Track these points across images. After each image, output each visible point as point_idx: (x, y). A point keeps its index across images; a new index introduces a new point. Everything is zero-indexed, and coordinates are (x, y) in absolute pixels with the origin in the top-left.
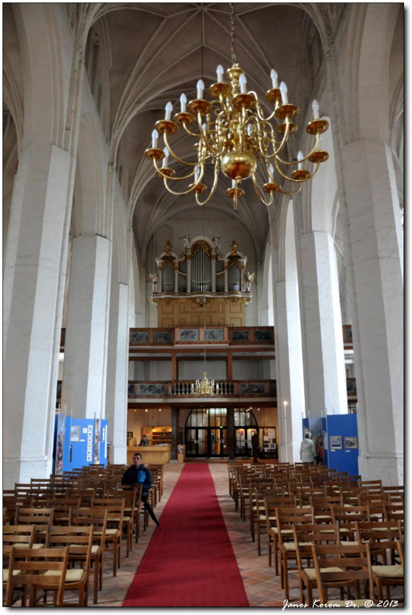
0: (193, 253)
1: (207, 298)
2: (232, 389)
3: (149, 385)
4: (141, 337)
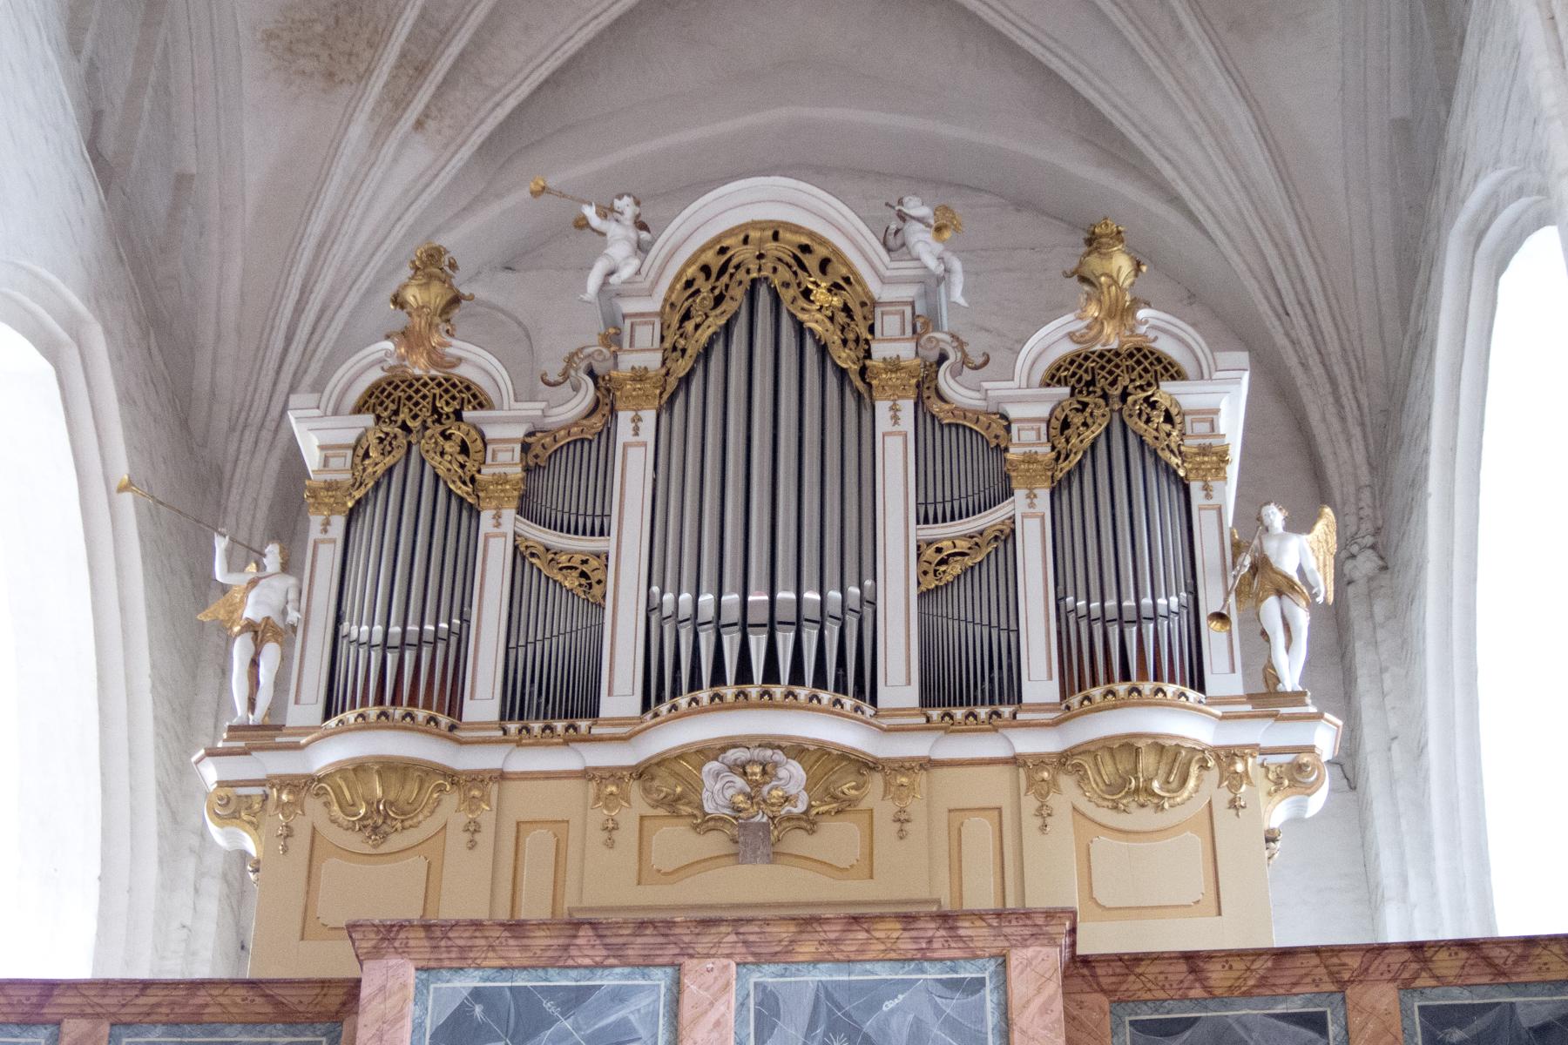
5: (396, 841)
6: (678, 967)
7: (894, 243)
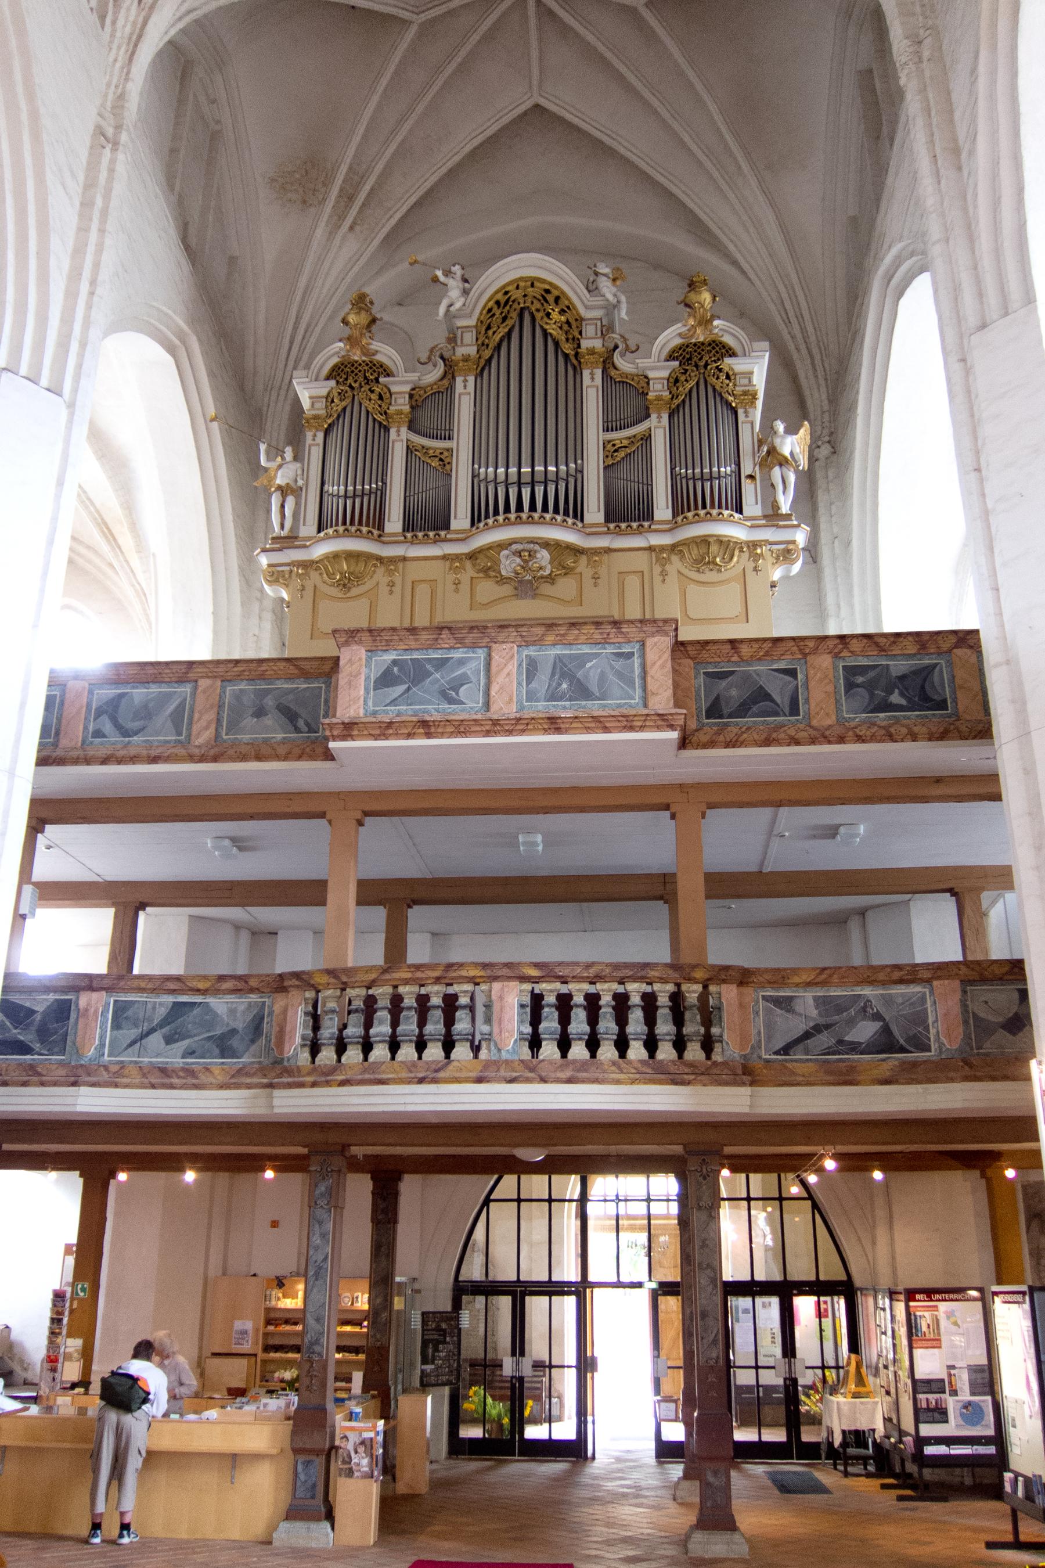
1: (556, 548)
2: (707, 1023)
3: (170, 999)
5: (355, 591)
6: (490, 648)
7: (592, 288)
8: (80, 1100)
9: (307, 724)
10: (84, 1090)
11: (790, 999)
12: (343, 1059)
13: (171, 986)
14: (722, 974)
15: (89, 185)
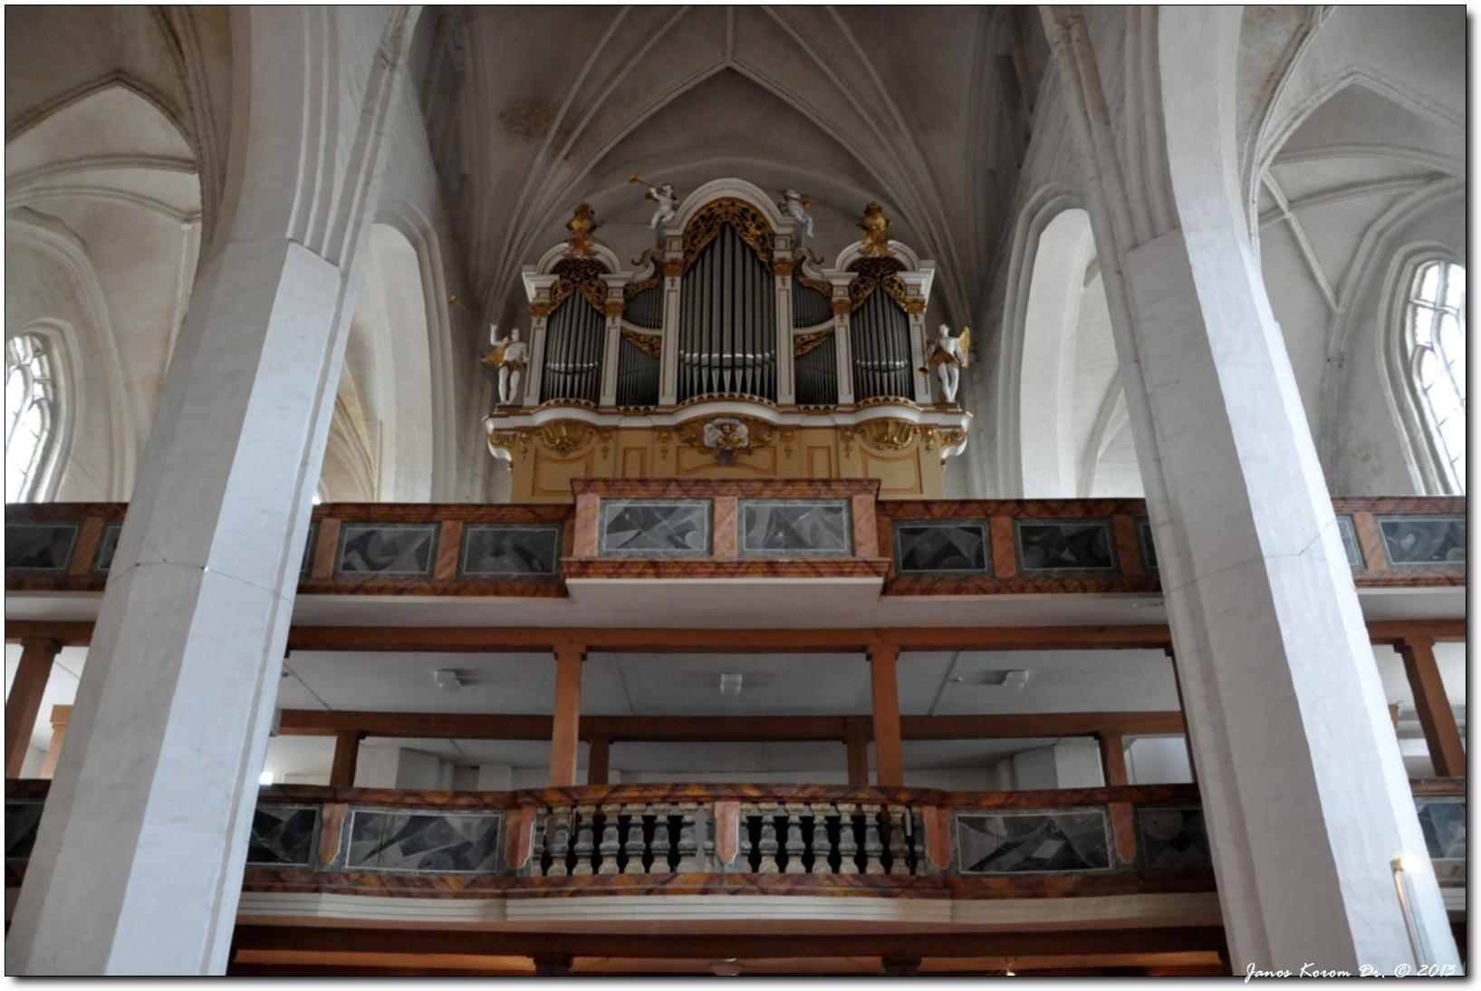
0: (687, 252)
2: (911, 841)
3: (408, 813)
4: (393, 549)
5: (572, 455)
6: (713, 500)
7: (784, 209)
8: (322, 906)
9: (541, 563)
10: (325, 896)
11: (984, 820)
12: (575, 872)
13: (410, 800)
14: (921, 797)
15: (370, 96)
